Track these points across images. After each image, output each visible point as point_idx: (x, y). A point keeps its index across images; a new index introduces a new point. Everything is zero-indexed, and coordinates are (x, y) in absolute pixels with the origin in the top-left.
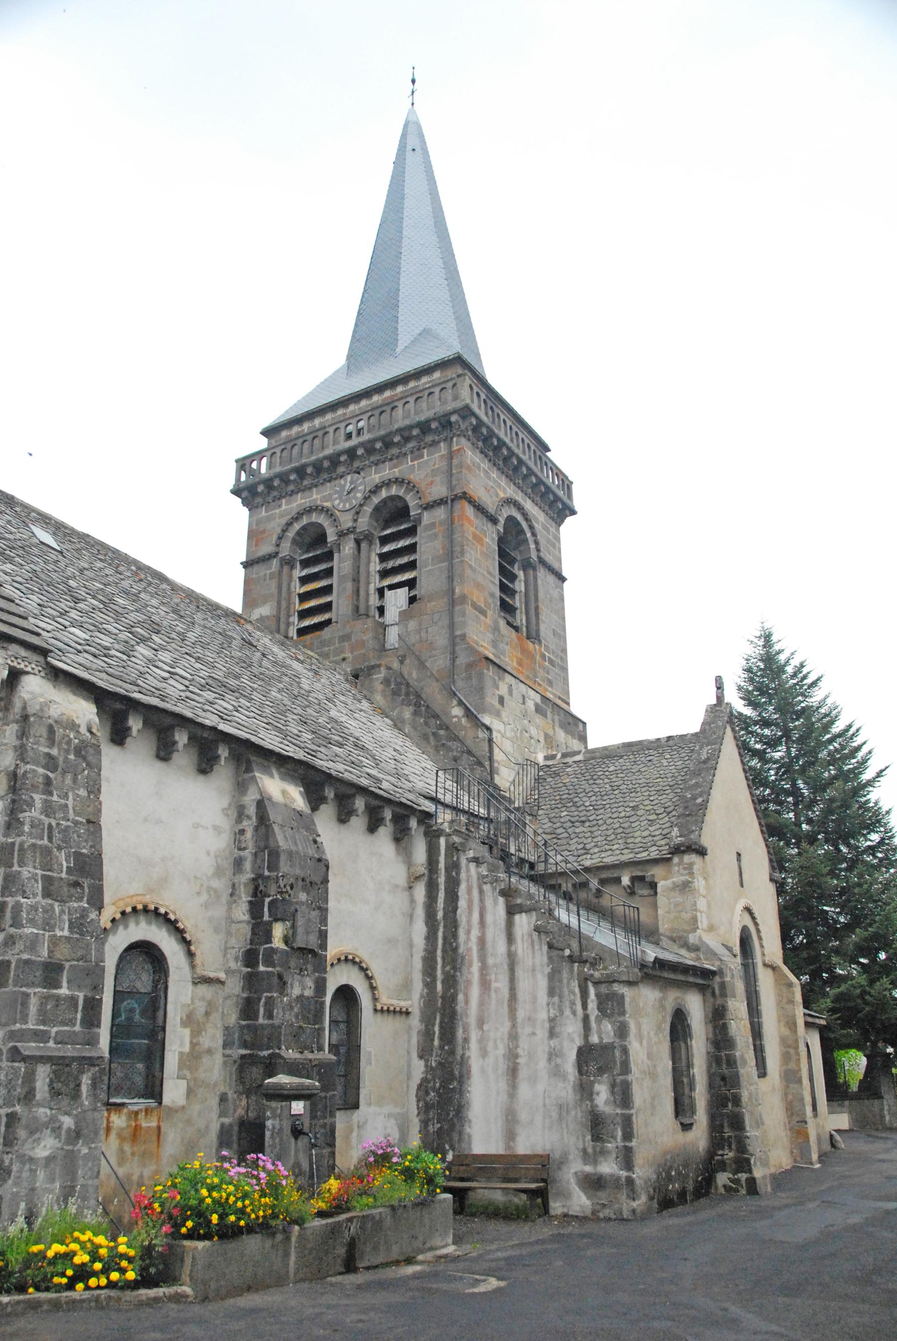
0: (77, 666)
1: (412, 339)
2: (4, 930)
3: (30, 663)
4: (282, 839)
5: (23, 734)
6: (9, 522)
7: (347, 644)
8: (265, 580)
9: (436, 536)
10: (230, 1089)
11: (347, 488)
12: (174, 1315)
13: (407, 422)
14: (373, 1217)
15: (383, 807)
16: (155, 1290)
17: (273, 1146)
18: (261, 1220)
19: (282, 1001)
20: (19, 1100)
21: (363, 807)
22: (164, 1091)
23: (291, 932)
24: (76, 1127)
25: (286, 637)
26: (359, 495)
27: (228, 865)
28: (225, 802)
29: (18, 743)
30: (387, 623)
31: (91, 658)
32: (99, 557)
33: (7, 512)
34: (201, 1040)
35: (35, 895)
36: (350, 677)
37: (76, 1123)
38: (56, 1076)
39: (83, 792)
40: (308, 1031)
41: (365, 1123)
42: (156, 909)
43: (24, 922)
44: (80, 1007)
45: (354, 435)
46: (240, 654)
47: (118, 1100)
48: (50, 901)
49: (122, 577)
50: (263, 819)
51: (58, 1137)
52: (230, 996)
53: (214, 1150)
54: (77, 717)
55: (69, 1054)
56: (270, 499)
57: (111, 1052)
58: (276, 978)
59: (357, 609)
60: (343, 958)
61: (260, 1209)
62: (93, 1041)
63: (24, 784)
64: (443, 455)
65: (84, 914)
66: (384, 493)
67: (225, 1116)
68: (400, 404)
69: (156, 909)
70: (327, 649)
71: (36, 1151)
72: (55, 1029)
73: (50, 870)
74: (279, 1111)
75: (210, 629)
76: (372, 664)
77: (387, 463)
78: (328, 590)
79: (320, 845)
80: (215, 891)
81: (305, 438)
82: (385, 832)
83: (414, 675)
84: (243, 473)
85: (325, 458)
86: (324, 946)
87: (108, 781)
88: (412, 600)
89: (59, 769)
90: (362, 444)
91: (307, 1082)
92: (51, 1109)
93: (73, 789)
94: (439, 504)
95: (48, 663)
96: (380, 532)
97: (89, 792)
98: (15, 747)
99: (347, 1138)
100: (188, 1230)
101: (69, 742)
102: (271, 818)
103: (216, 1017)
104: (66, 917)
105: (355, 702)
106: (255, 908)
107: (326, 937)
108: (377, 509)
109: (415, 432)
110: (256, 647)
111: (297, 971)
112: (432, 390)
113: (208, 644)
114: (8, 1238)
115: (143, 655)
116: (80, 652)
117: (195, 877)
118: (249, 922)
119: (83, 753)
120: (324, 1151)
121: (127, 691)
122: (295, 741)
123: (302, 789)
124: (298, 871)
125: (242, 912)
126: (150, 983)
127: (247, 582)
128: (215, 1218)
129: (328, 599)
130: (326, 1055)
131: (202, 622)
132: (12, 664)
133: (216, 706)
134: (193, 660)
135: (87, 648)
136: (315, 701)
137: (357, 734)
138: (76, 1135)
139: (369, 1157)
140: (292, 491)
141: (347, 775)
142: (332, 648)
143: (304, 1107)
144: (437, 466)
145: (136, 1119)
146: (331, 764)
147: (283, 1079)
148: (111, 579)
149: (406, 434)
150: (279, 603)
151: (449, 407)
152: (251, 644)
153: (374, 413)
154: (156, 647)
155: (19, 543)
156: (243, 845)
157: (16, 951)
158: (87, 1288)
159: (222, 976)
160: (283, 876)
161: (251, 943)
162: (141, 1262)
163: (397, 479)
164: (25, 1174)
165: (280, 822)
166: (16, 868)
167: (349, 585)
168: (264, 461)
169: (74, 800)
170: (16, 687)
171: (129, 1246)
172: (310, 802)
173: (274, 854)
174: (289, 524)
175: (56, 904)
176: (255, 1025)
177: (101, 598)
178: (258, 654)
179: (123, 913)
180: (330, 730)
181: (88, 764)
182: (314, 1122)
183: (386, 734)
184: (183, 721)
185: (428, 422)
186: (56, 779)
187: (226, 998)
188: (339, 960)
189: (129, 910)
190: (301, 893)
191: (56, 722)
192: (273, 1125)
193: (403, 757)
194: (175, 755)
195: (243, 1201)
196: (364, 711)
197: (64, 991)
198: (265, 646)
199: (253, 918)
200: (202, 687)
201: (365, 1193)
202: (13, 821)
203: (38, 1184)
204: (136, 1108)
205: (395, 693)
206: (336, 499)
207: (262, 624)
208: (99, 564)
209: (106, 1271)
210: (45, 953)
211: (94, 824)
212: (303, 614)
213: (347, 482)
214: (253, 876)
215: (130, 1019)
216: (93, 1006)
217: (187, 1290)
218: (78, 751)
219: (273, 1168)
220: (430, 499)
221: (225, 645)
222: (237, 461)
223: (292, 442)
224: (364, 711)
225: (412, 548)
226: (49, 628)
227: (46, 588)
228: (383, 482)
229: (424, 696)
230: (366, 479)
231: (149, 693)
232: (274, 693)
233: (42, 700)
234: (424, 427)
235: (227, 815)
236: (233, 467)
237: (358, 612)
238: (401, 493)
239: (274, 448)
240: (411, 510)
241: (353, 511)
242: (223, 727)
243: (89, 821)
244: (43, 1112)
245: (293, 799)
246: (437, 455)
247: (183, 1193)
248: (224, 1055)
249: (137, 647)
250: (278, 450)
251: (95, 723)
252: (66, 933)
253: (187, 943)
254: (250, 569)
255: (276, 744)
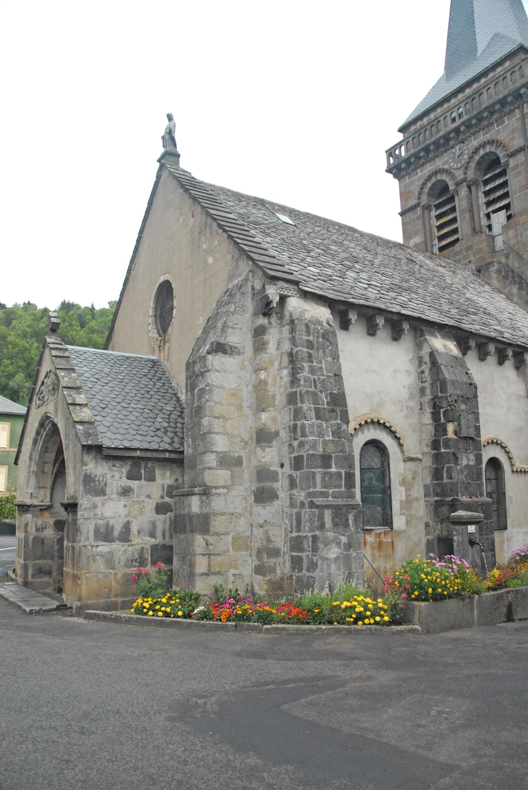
0: (316, 288)
1: (487, 43)
2: (298, 439)
3: (290, 290)
4: (447, 374)
5: (292, 331)
6: (264, 214)
7: (470, 252)
8: (414, 221)
9: (519, 173)
10: (430, 519)
11: (457, 154)
12: (412, 640)
13: (491, 102)
14: (522, 592)
15: (507, 348)
16: (400, 626)
17: (459, 551)
18: (456, 591)
19: (456, 468)
20: (317, 528)
21: (494, 350)
22: (394, 522)
23: (458, 428)
24: (349, 542)
25: (433, 254)
26: (466, 157)
27: (416, 392)
28: (410, 356)
29: (291, 336)
30: (494, 235)
31: (323, 283)
32: (317, 224)
33: (262, 208)
34: (412, 493)
35: (311, 419)
36: (475, 272)
37: (348, 540)
38: (335, 516)
39: (329, 359)
40: (474, 485)
41: (512, 537)
42: (378, 421)
43: (308, 433)
44: (343, 478)
45: (457, 118)
46: (407, 268)
47: (369, 528)
48: (320, 421)
49: (331, 234)
50: (434, 363)
51: (340, 547)
52: (425, 468)
53: (424, 554)
54: (321, 317)
55: (340, 503)
56: (410, 171)
57: (362, 502)
58: (452, 455)
59: (474, 229)
60: (490, 442)
61: (455, 586)
62: (352, 496)
63: (297, 358)
64: (518, 119)
65: (339, 427)
66: (482, 152)
67: (430, 535)
68: (484, 91)
69: (378, 421)
70: (458, 257)
71: (329, 554)
72: (331, 491)
73: (317, 404)
74: (461, 531)
75: (387, 255)
76: (488, 261)
77: (481, 132)
78: (454, 220)
79: (470, 375)
80: (411, 408)
81: (426, 128)
82: (509, 364)
83: (516, 264)
84: (391, 158)
85: (441, 138)
86: (479, 435)
87: (343, 351)
88: (509, 217)
89: (315, 347)
90: (463, 124)
91: (476, 514)
92: (334, 533)
93: (324, 358)
94: (520, 151)
95: (300, 289)
96: (482, 178)
97: (333, 359)
98: (289, 338)
99: (501, 547)
100: (416, 596)
101: (318, 332)
102: (439, 362)
103: (418, 479)
104: (330, 429)
105: (481, 287)
106: (435, 416)
107: (479, 429)
108: (479, 163)
109: (497, 107)
110: (415, 262)
111: (464, 451)
112: (505, 75)
113: (387, 264)
114: (321, 598)
115: (351, 277)
116: (316, 280)
117: (398, 401)
118: (432, 424)
119: (326, 337)
120: (489, 554)
121: (346, 298)
122: (447, 315)
123: (455, 343)
124: (459, 392)
125: (427, 419)
126: (380, 462)
127: (404, 224)
128: (430, 591)
129: (455, 226)
130: (485, 499)
131: (382, 252)
132: (280, 293)
133: (398, 300)
134: (380, 275)
135: (319, 277)
136: (457, 290)
137: (484, 306)
138: (349, 546)
139: (516, 557)
140: (423, 163)
141: (482, 332)
142: (461, 256)
143: (475, 529)
144: (515, 126)
145: (380, 538)
146: (471, 326)
147: (461, 513)
148: (325, 236)
149: (491, 110)
150: (425, 234)
151: (518, 85)
152: (412, 261)
153: (468, 100)
154: (358, 271)
155: (272, 225)
156: (424, 380)
157: (306, 449)
158: (364, 624)
159: (420, 456)
160: (450, 396)
161: (435, 435)
162: (391, 612)
163: (489, 141)
164: (325, 566)
165: (445, 364)
166: (299, 405)
167: (467, 215)
168: (403, 148)
169: (326, 364)
170: (285, 305)
171: (384, 603)
172: (461, 350)
173: (443, 383)
174: (424, 184)
175: (324, 422)
176: (442, 483)
177: (322, 247)
178: (418, 266)
179: (360, 425)
180: (467, 306)
181: (330, 343)
182: (481, 537)
183: (503, 304)
184: (380, 311)
185: (505, 98)
186: (314, 353)
187: (423, 469)
188: (488, 443)
189: (363, 423)
190: (462, 405)
191: (309, 321)
192: (458, 539)
193: (515, 317)
194: (378, 332)
195: (445, 581)
196: (487, 292)
197: (334, 470)
198: (421, 261)
199: (435, 422)
200: (388, 290)
201: (516, 577)
202: (294, 380)
203: (332, 572)
204: (379, 532)
205: (505, 278)
206: (451, 163)
207: (417, 248)
208: (317, 229)
209: (373, 616)
210: (321, 450)
211: (338, 376)
212: (441, 238)
213: (457, 150)
214: (432, 397)
215: (370, 484)
216: (350, 477)
217: (418, 627)
218: (324, 336)
219: (460, 563)
220: (512, 149)
221: (397, 264)
222: (386, 152)
223: (418, 132)
224: (487, 292)
225: (505, 184)
226: (297, 269)
227: (291, 247)
228: (432, 173)
229: (524, 277)
230: (469, 146)
231: (358, 298)
232: (431, 288)
233: (300, 310)
234: (503, 102)
235: (413, 363)
236: (385, 156)
237: (475, 231)
238: (493, 150)
239: (408, 138)
240: (501, 159)
241: (463, 168)
242: (403, 311)
243: (335, 375)
244: (330, 535)
245: (450, 349)
246: (514, 119)
247: (411, 576)
248: (425, 501)
249: (347, 273)
250: (410, 139)
251: (331, 319)
252: (331, 438)
253: (398, 439)
254: (404, 216)
255: (436, 318)
